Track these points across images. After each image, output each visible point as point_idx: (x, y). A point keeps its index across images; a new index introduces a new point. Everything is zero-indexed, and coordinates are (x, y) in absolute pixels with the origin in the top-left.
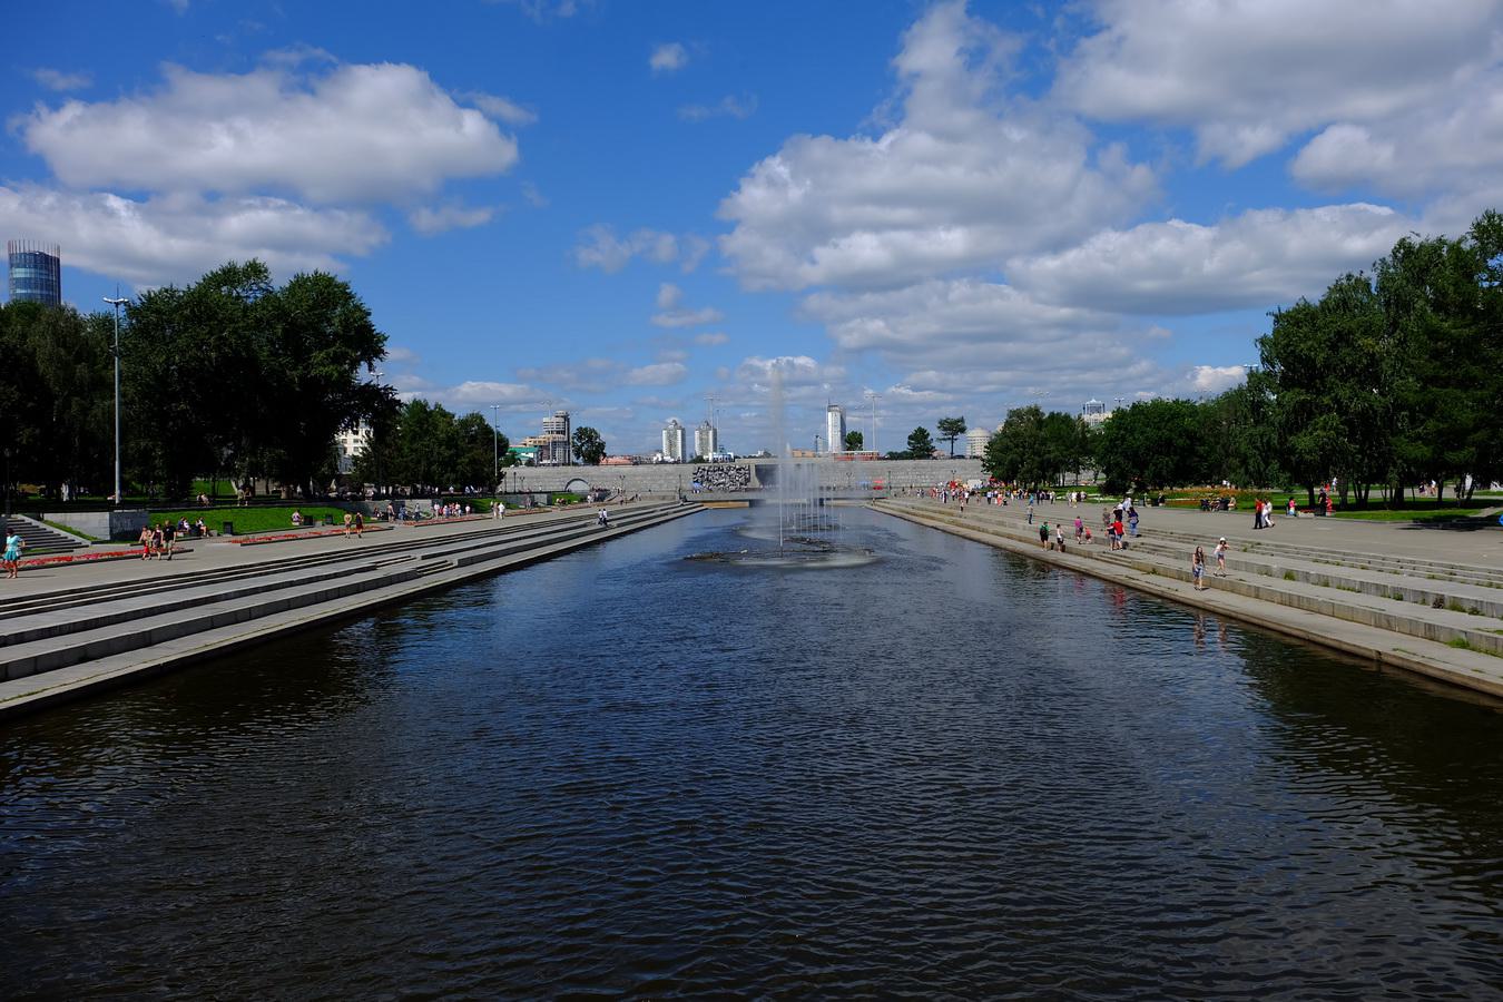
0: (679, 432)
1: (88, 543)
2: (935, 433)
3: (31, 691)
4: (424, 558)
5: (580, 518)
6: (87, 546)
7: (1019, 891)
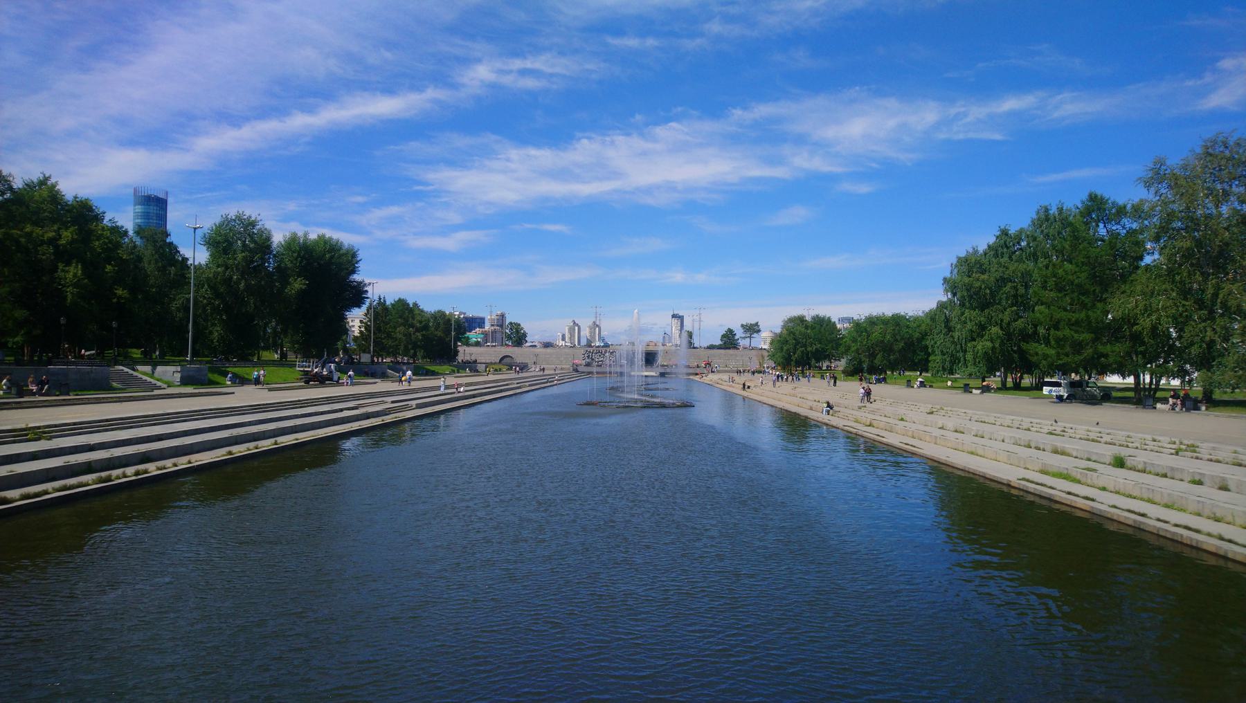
0: (576, 328)
1: (165, 386)
2: (739, 333)
3: (914, 445)
4: (393, 402)
5: (504, 380)
6: (164, 389)
7: (786, 638)
